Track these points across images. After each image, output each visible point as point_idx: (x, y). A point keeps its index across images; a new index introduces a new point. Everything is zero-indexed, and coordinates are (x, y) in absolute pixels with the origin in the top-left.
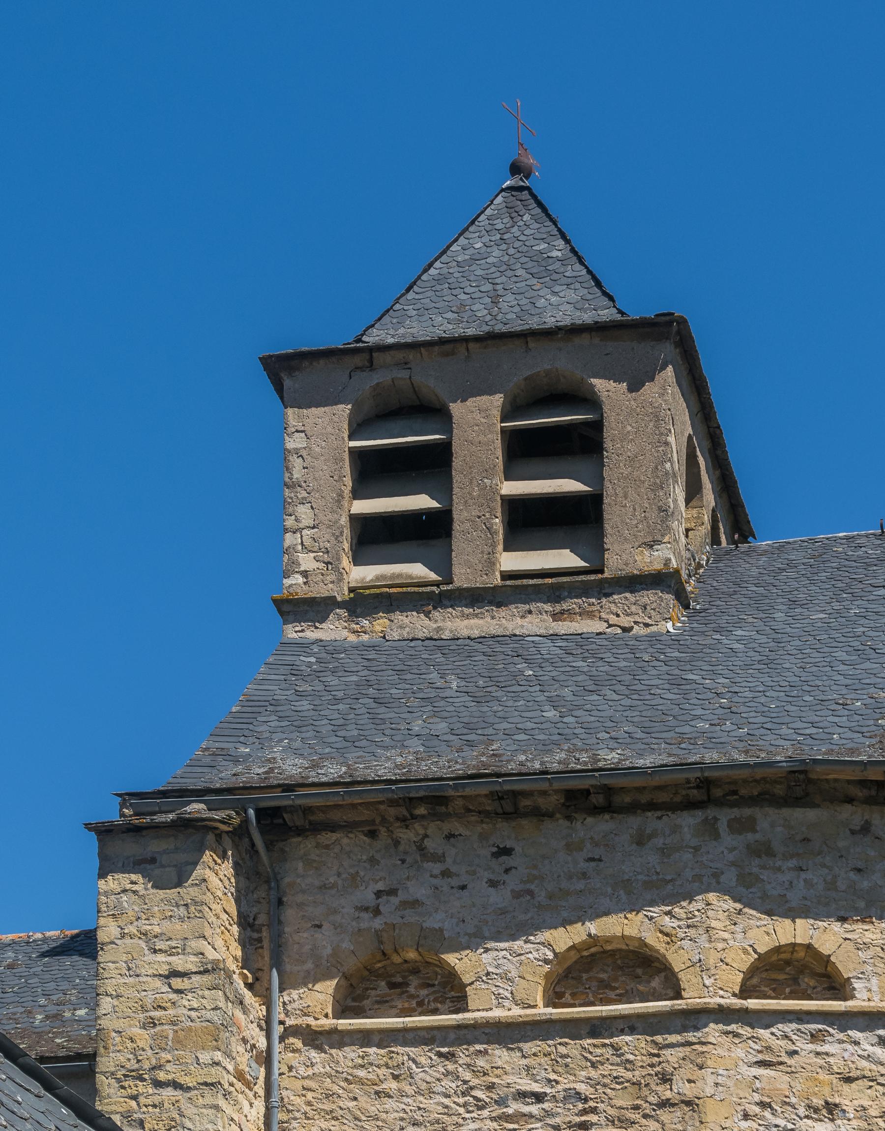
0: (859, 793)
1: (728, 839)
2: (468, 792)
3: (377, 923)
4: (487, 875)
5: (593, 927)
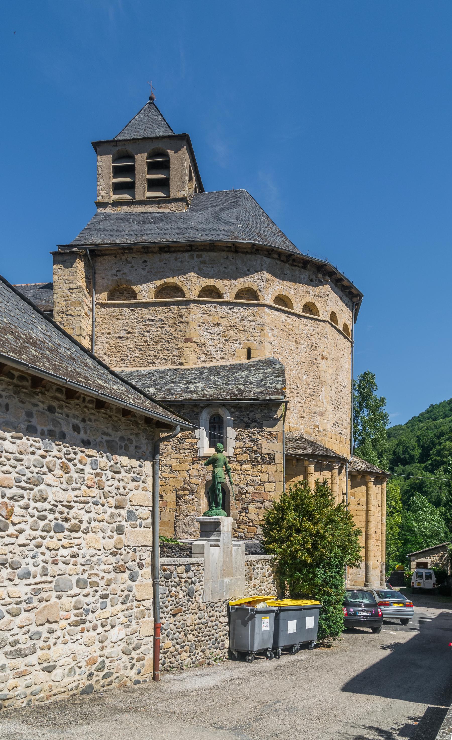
0: (226, 249)
1: (196, 260)
2: (137, 247)
3: (117, 278)
4: (141, 267)
5: (165, 280)
